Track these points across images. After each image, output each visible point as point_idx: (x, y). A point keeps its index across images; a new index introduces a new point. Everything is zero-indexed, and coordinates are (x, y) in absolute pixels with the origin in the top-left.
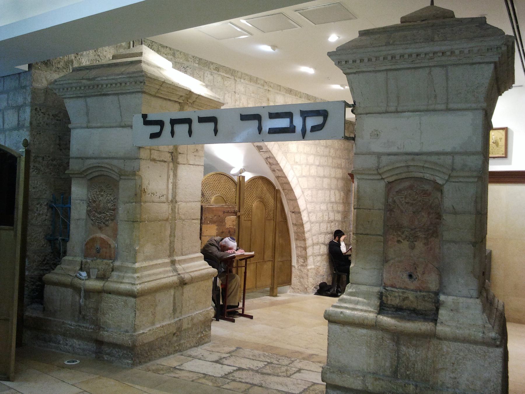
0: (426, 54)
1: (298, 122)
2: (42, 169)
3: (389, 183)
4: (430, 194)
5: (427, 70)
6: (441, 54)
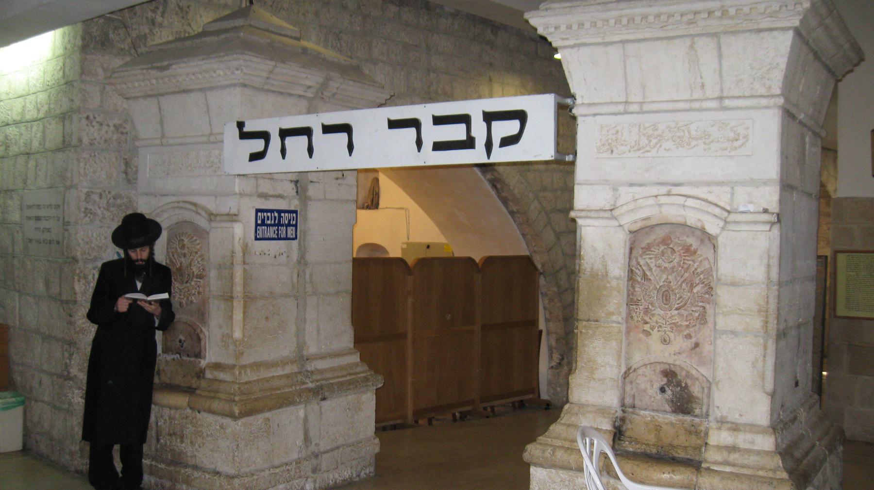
0: (682, 15)
1: (479, 130)
2: (99, 212)
4: (695, 252)
5: (688, 41)
6: (706, 15)
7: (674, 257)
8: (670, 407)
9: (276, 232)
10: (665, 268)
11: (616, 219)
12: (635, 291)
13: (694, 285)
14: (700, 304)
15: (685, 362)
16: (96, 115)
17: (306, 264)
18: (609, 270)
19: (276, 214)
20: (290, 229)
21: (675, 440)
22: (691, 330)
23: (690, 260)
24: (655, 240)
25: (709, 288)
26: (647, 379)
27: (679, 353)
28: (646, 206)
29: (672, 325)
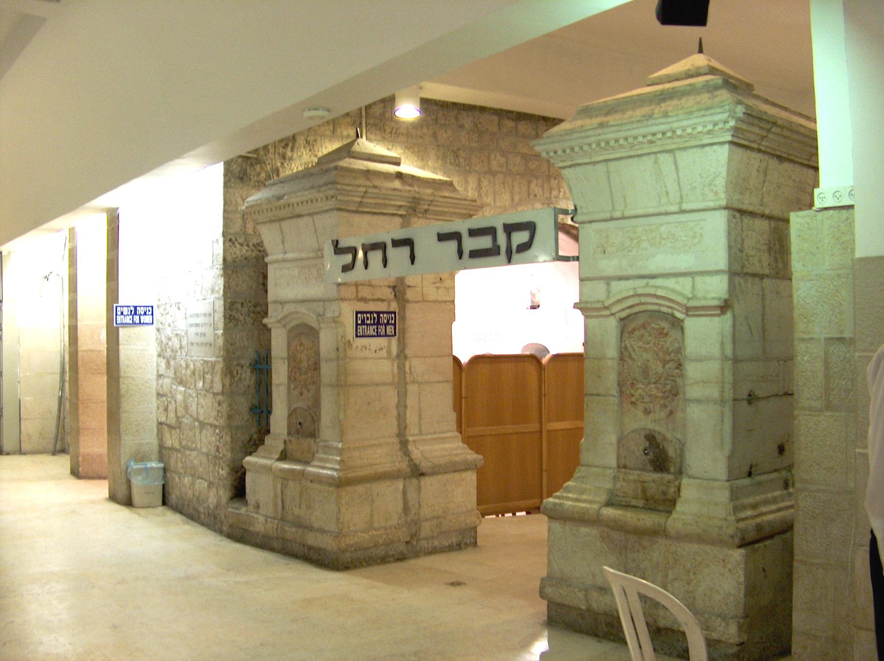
2: (242, 319)
3: (622, 320)
9: (376, 330)
16: (237, 238)
17: (406, 357)
19: (375, 315)
20: (388, 328)
25: (679, 365)
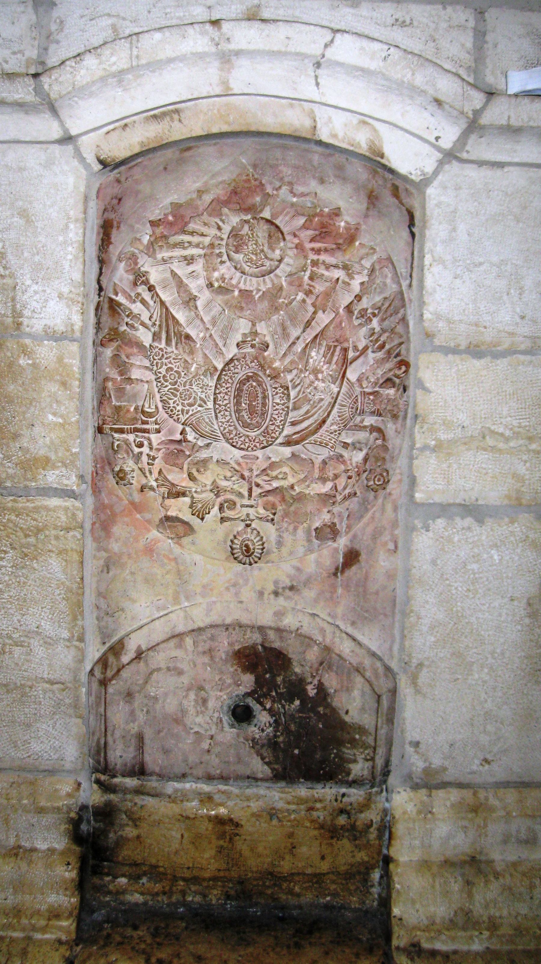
7: (278, 252)
8: (268, 764)
10: (246, 294)
11: (53, 110)
12: (129, 380)
13: (351, 354)
14: (369, 421)
15: (314, 615)
18: (24, 306)
21: (283, 859)
22: (336, 509)
23: (336, 266)
24: (200, 192)
26: (185, 680)
27: (292, 588)
28: (170, 60)
29: (270, 498)
